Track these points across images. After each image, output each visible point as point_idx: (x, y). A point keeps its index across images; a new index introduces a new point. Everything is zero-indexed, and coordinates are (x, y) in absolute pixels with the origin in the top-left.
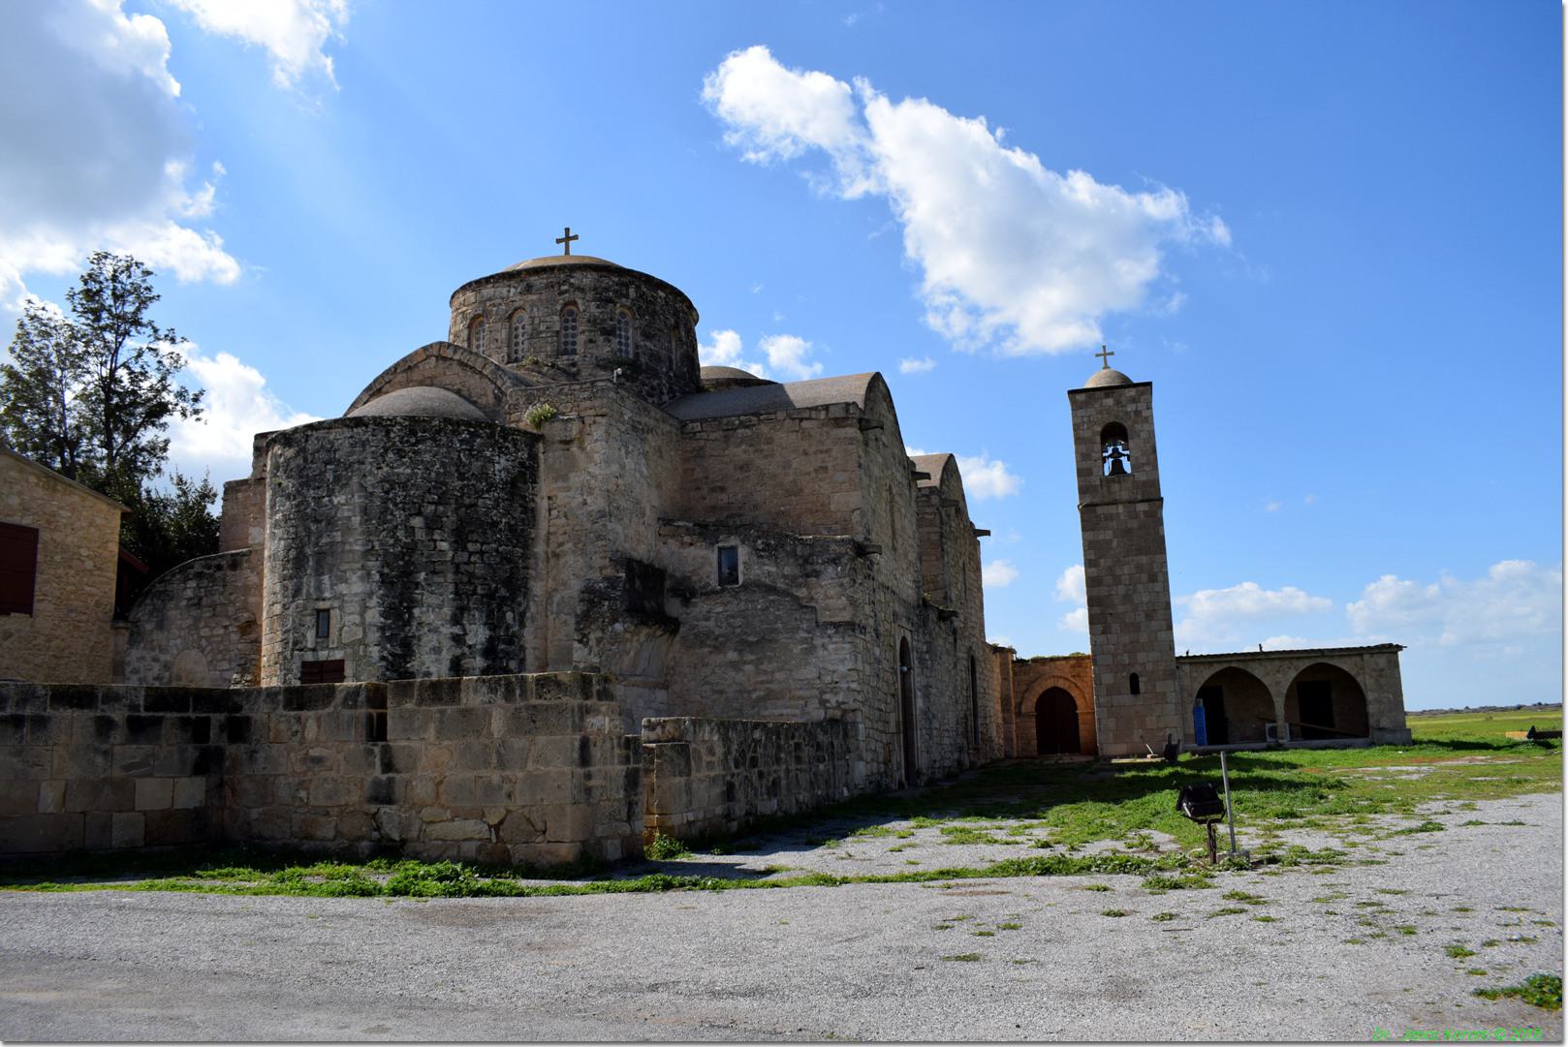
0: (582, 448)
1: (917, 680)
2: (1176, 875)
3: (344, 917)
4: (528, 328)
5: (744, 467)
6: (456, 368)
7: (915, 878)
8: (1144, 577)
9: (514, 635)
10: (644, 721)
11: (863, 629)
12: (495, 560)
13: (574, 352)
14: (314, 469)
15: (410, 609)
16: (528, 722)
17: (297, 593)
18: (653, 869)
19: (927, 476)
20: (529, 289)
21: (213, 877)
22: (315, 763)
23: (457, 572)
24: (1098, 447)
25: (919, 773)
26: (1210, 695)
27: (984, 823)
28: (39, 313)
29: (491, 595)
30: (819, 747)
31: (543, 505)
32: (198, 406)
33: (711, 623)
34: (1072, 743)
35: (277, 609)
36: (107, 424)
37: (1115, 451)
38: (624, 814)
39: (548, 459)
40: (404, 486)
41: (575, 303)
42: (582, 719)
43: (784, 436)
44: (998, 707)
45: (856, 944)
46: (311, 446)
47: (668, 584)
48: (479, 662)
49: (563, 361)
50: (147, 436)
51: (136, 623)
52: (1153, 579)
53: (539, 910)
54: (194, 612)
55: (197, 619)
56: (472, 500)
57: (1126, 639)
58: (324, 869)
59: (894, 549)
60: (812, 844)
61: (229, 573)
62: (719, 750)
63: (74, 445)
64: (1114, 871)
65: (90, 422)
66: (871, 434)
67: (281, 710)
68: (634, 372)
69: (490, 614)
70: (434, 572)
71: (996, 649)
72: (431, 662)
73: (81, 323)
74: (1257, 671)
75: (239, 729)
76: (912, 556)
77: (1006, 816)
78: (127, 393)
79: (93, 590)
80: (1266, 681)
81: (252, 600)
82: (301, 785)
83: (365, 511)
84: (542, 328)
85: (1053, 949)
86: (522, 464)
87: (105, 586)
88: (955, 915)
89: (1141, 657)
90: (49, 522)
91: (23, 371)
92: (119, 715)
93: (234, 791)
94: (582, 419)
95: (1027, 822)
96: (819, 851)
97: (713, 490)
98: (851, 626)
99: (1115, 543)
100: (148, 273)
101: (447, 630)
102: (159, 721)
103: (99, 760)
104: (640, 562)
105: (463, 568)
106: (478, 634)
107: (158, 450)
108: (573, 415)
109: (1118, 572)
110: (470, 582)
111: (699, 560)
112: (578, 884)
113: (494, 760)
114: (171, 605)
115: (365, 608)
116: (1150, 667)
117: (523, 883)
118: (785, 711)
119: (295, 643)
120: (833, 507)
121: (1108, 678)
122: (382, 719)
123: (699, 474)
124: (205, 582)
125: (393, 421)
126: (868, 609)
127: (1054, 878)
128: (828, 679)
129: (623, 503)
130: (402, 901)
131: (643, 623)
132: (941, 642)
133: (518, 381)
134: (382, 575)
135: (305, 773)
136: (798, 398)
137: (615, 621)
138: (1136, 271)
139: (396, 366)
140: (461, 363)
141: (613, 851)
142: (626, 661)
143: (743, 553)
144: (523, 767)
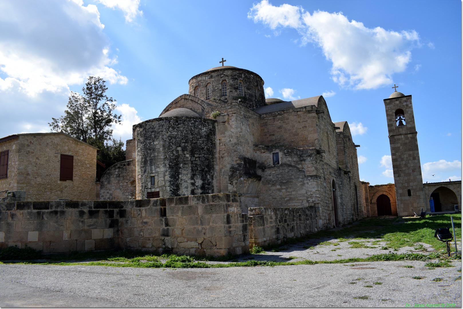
0: (229, 124)
1: (338, 193)
2: (436, 261)
3: (147, 276)
4: (212, 89)
5: (280, 127)
6: (190, 102)
7: (341, 262)
8: (411, 158)
9: (210, 182)
10: (249, 208)
11: (320, 177)
12: (203, 159)
13: (226, 95)
14: (149, 134)
15: (178, 175)
16: (209, 210)
17: (145, 171)
18: (252, 257)
19: (339, 128)
20: (211, 77)
21: (113, 260)
22: (145, 224)
23: (192, 163)
24: (394, 117)
25: (340, 223)
26: (435, 196)
27: (363, 240)
28: (75, 95)
29: (203, 170)
30: (307, 215)
31: (218, 142)
32: (120, 120)
33: (271, 177)
34: (389, 213)
35: (140, 177)
36: (95, 126)
37: (400, 118)
38: (242, 239)
39: (218, 128)
40: (175, 138)
41: (225, 80)
42: (227, 209)
43: (292, 117)
44: (364, 201)
45: (321, 290)
46: (147, 127)
47: (257, 165)
48: (200, 191)
49: (223, 98)
50: (106, 128)
51: (102, 182)
52: (414, 158)
53: (211, 273)
54: (118, 179)
55: (119, 181)
56: (196, 141)
57: (406, 178)
58: (147, 257)
59: (329, 151)
60: (305, 248)
61: (127, 166)
62: (274, 218)
63: (86, 132)
64: (413, 259)
65: (90, 125)
66: (320, 115)
67: (135, 208)
68: (245, 100)
69: (202, 176)
70: (185, 164)
71: (363, 183)
72: (185, 191)
73: (86, 97)
74: (451, 188)
75: (122, 213)
76: (335, 154)
77: (370, 238)
78: (100, 116)
79: (90, 173)
80: (454, 191)
81: (134, 174)
82: (141, 231)
83: (164, 146)
84: (216, 88)
85: (396, 294)
86: (210, 130)
87: (93, 172)
88: (357, 278)
89: (411, 184)
90: (76, 154)
91: (72, 112)
92: (86, 210)
93: (122, 233)
94: (228, 115)
95: (378, 240)
96: (308, 250)
97: (270, 135)
98: (316, 176)
99: (401, 148)
100: (104, 82)
101: (190, 181)
102: (98, 211)
103: (81, 224)
104: (248, 159)
105: (194, 162)
106: (199, 182)
107: (109, 133)
108: (226, 114)
109: (402, 157)
110: (196, 166)
111: (267, 157)
112: (226, 263)
113: (199, 222)
114: (112, 176)
115: (165, 176)
116: (414, 187)
117: (209, 263)
118: (296, 204)
119: (145, 187)
120: (309, 139)
121: (400, 191)
122: (165, 209)
123: (266, 130)
124: (121, 170)
125: (171, 118)
126: (321, 171)
127: (390, 262)
128: (309, 193)
129: (242, 140)
130: (168, 270)
131: (250, 177)
132: (345, 181)
133: (209, 104)
134: (169, 165)
135: (142, 227)
136: (296, 105)
137: (241, 177)
138: (402, 61)
139: (172, 102)
140: (191, 100)
141: (239, 251)
142: (245, 189)
143: (280, 155)
144: (209, 225)
